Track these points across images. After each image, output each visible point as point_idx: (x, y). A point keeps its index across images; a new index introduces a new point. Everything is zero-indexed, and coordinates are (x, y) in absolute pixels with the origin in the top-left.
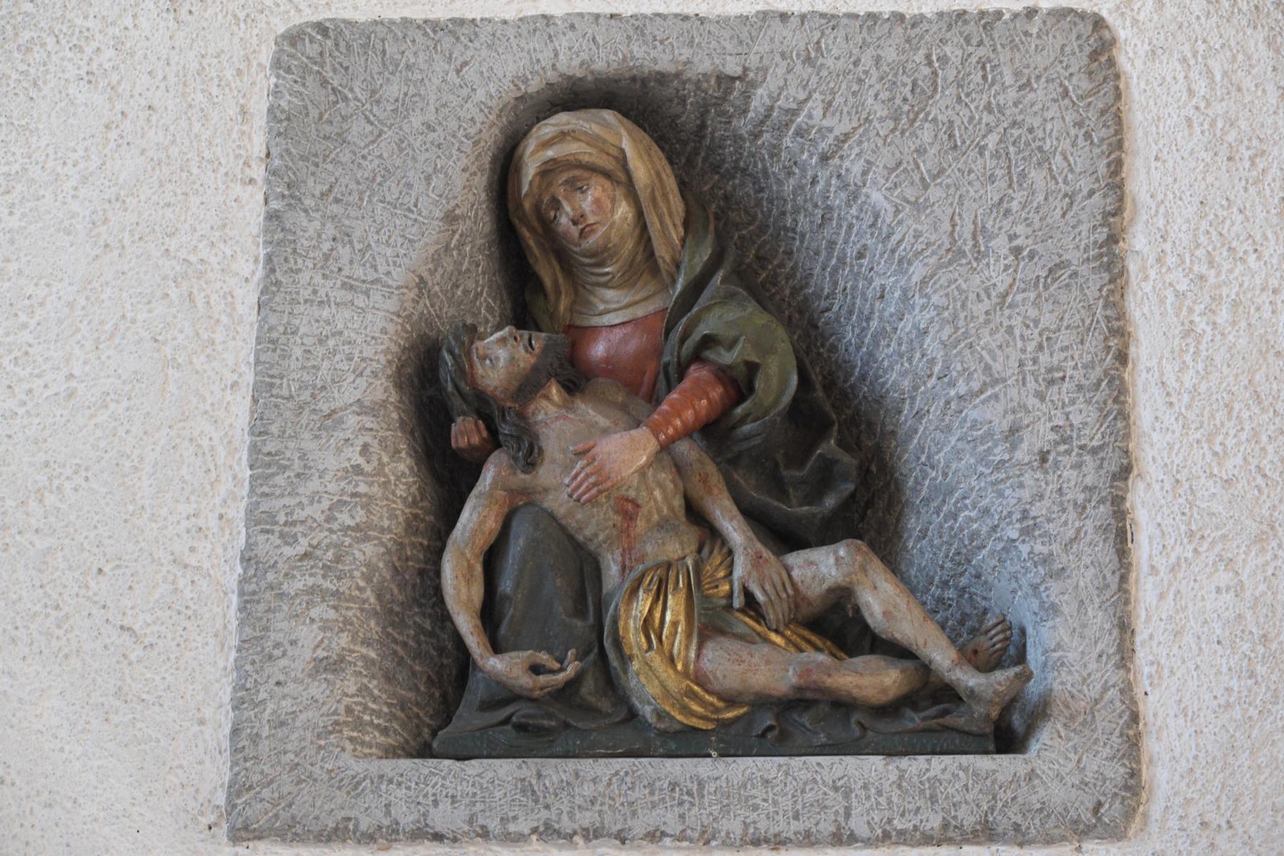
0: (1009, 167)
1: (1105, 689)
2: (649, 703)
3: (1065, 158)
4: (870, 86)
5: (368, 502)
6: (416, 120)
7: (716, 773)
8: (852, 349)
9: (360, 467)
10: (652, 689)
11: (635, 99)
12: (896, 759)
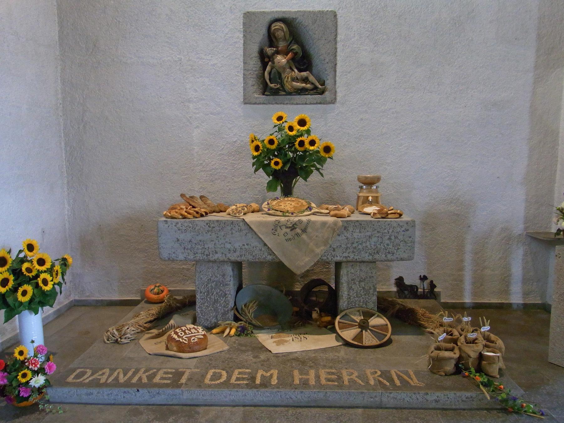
9: (255, 63)
11: (283, 20)
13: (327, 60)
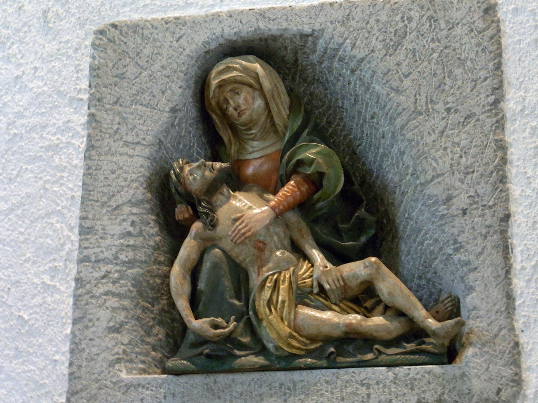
0: (443, 69)
1: (500, 330)
2: (272, 342)
3: (472, 62)
4: (374, 34)
5: (134, 248)
6: (157, 66)
7: (302, 378)
8: (372, 163)
9: (131, 227)
10: (273, 335)
11: (262, 48)
12: (393, 369)
13: (461, 201)
